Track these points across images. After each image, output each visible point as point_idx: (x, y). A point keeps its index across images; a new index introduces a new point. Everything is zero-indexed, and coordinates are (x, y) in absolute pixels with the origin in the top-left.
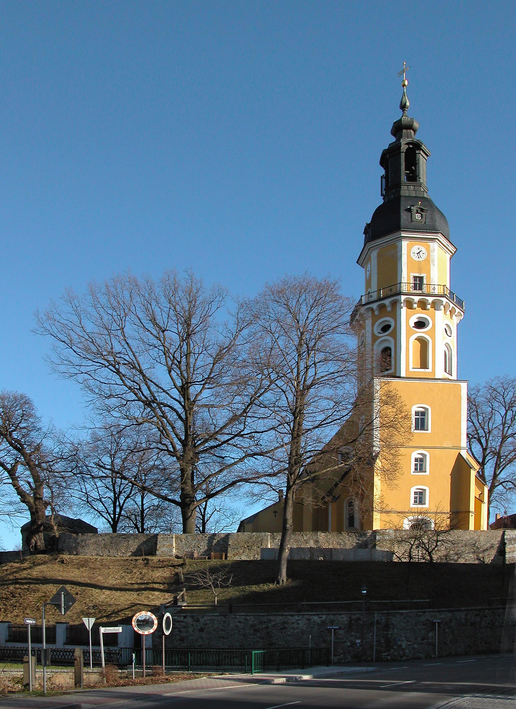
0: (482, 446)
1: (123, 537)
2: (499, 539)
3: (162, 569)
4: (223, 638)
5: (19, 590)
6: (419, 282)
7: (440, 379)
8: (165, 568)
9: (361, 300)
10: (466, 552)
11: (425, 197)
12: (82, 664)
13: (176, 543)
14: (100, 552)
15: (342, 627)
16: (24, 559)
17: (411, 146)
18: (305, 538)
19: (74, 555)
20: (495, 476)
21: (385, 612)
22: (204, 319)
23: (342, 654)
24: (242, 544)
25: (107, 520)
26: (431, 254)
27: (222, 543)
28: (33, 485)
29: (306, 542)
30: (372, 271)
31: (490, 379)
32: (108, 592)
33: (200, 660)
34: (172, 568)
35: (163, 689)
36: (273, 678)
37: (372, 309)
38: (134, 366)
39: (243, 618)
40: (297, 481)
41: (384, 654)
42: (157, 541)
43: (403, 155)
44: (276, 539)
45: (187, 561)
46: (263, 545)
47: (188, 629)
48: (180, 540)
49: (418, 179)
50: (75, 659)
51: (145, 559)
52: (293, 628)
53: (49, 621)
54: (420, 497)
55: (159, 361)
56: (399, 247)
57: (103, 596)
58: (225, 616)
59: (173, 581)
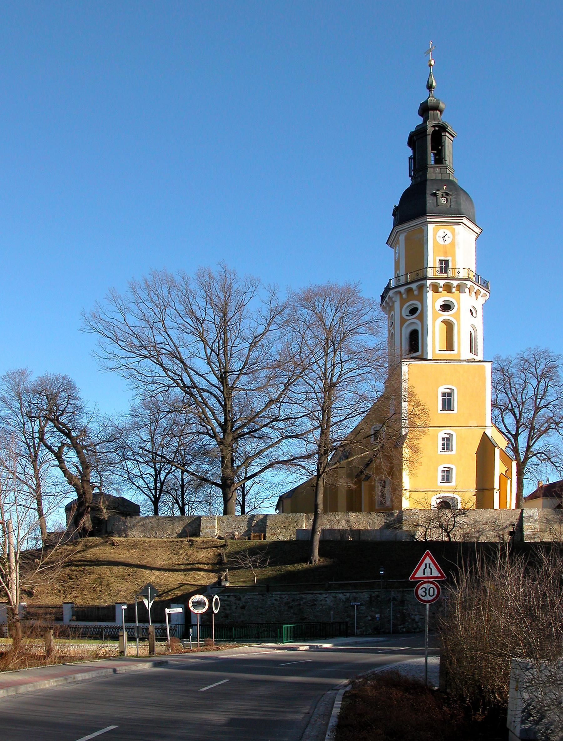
0: (515, 417)
1: (169, 519)
2: (518, 517)
3: (206, 550)
4: (262, 614)
5: (75, 573)
6: (444, 265)
7: (465, 361)
8: (209, 549)
9: (389, 283)
10: (487, 530)
11: (451, 180)
12: (155, 640)
13: (218, 525)
14: (148, 534)
15: (364, 603)
16: (76, 542)
17: (437, 129)
19: (123, 537)
20: (529, 447)
21: (401, 589)
22: (240, 307)
23: (363, 627)
24: (279, 524)
25: (148, 496)
26: (456, 237)
27: (261, 524)
28: (80, 467)
29: (339, 522)
30: (400, 253)
31: (521, 351)
32: (157, 573)
33: (242, 634)
34: (216, 549)
35: (220, 654)
36: (298, 646)
37: (400, 292)
38: (175, 355)
40: (327, 470)
41: (400, 627)
42: (200, 522)
43: (429, 138)
45: (229, 541)
46: (299, 525)
49: (444, 162)
50: (150, 634)
51: (190, 540)
52: (321, 605)
53: (106, 602)
54: (447, 476)
55: (198, 355)
56: (425, 231)
57: (154, 577)
58: (263, 595)
59: (216, 561)
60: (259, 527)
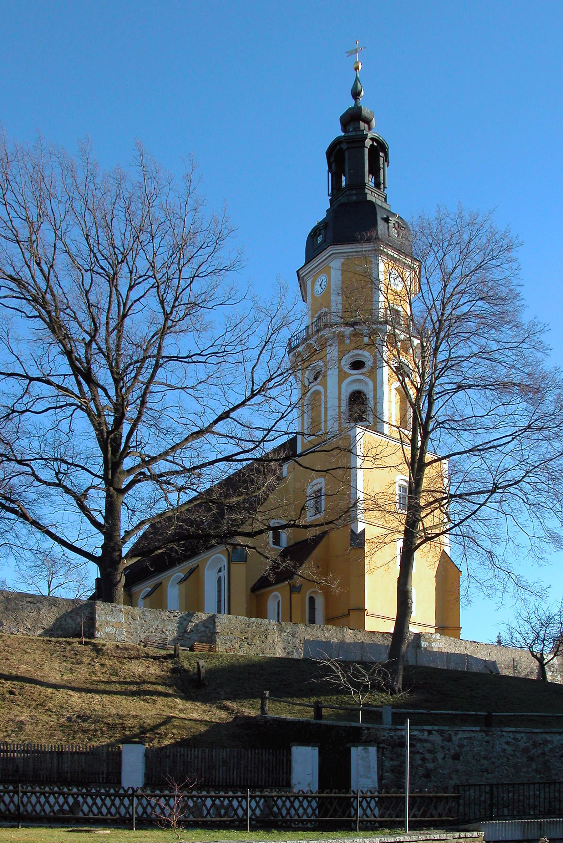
17: (375, 144)
18: (326, 635)
24: (237, 633)
39: (512, 737)
43: (366, 151)
44: (285, 632)
47: (436, 754)
48: (132, 617)
60: (200, 635)
